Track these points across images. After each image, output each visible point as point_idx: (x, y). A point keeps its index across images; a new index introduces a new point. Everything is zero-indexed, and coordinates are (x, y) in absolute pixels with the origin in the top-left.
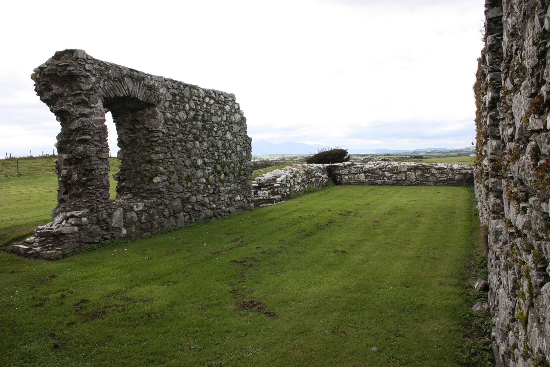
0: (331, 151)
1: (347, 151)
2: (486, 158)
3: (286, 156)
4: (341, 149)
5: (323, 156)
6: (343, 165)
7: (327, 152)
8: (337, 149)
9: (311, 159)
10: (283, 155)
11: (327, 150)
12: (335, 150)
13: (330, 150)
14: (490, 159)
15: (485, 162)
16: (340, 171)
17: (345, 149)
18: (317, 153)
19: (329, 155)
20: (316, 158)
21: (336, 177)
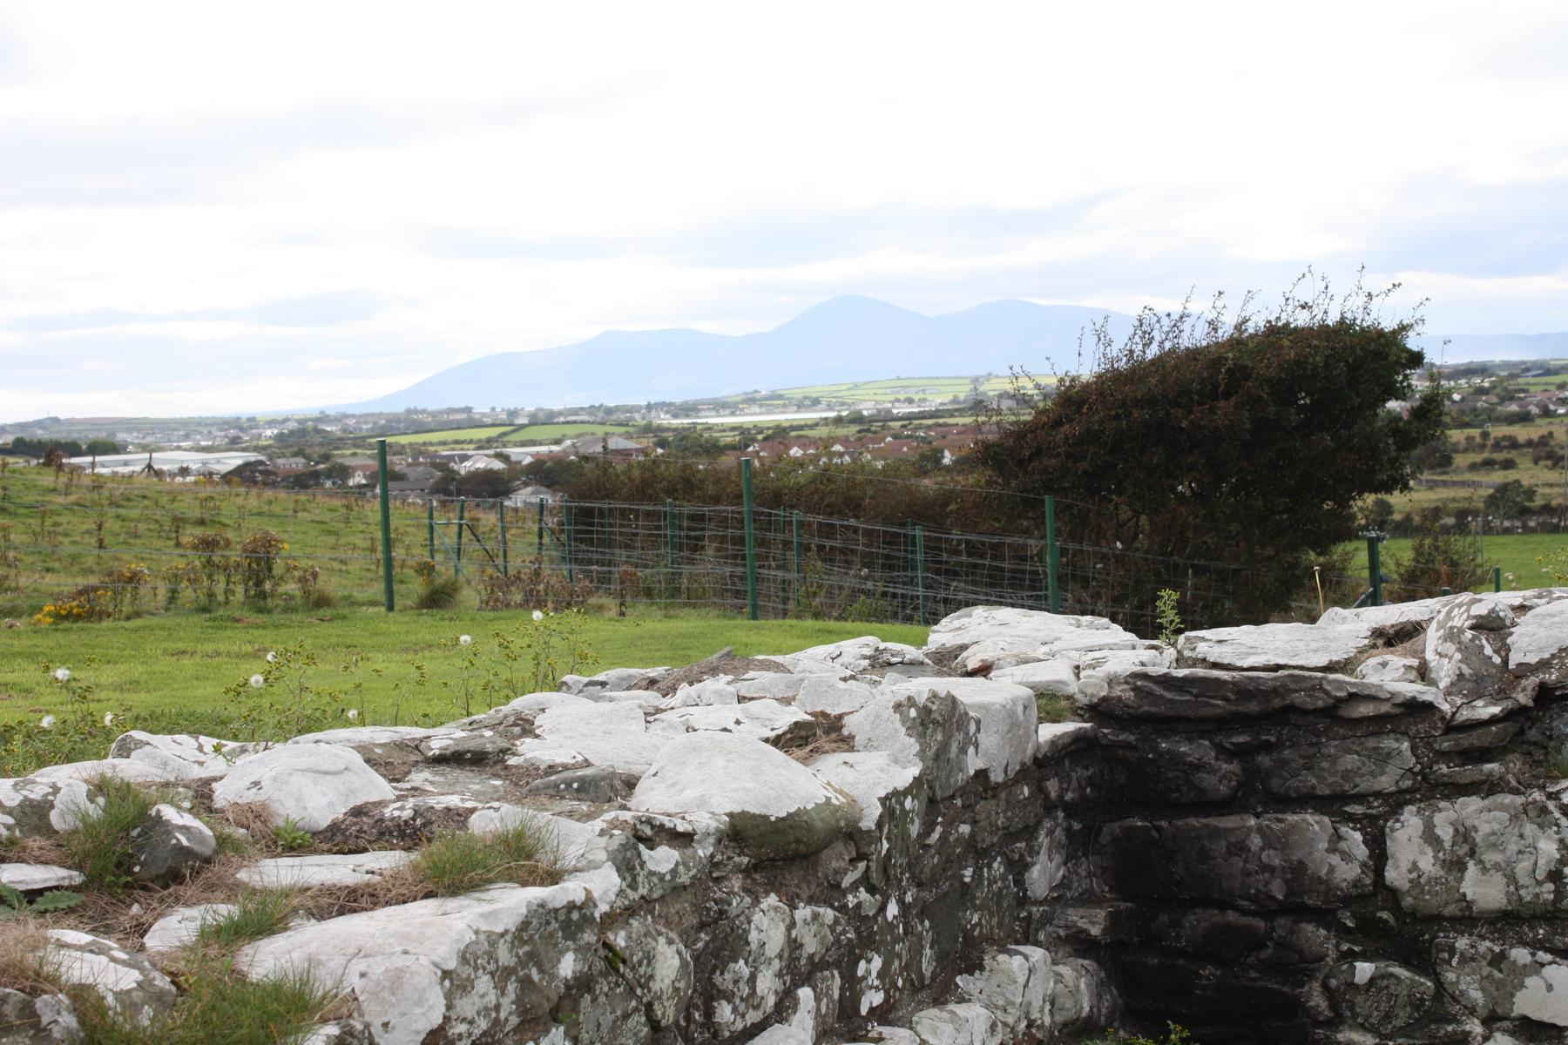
0: (1236, 342)
1: (1412, 343)
2: (513, 978)
3: (991, 389)
4: (1344, 326)
5: (1151, 402)
6: (1472, 685)
7: (1193, 354)
8: (1302, 319)
9: (1021, 433)
10: (976, 380)
11: (1195, 336)
12: (1275, 332)
13: (1226, 331)
14: (638, 779)
15: (816, 496)
16: (1406, 833)
17: (1388, 324)
18: (1087, 369)
19: (1211, 393)
20: (1073, 429)
21: (1300, 966)
